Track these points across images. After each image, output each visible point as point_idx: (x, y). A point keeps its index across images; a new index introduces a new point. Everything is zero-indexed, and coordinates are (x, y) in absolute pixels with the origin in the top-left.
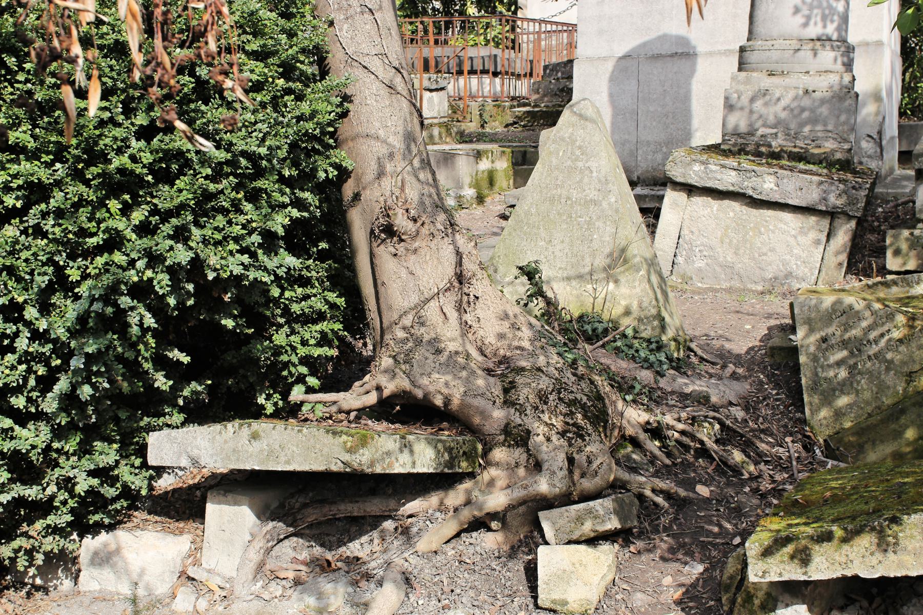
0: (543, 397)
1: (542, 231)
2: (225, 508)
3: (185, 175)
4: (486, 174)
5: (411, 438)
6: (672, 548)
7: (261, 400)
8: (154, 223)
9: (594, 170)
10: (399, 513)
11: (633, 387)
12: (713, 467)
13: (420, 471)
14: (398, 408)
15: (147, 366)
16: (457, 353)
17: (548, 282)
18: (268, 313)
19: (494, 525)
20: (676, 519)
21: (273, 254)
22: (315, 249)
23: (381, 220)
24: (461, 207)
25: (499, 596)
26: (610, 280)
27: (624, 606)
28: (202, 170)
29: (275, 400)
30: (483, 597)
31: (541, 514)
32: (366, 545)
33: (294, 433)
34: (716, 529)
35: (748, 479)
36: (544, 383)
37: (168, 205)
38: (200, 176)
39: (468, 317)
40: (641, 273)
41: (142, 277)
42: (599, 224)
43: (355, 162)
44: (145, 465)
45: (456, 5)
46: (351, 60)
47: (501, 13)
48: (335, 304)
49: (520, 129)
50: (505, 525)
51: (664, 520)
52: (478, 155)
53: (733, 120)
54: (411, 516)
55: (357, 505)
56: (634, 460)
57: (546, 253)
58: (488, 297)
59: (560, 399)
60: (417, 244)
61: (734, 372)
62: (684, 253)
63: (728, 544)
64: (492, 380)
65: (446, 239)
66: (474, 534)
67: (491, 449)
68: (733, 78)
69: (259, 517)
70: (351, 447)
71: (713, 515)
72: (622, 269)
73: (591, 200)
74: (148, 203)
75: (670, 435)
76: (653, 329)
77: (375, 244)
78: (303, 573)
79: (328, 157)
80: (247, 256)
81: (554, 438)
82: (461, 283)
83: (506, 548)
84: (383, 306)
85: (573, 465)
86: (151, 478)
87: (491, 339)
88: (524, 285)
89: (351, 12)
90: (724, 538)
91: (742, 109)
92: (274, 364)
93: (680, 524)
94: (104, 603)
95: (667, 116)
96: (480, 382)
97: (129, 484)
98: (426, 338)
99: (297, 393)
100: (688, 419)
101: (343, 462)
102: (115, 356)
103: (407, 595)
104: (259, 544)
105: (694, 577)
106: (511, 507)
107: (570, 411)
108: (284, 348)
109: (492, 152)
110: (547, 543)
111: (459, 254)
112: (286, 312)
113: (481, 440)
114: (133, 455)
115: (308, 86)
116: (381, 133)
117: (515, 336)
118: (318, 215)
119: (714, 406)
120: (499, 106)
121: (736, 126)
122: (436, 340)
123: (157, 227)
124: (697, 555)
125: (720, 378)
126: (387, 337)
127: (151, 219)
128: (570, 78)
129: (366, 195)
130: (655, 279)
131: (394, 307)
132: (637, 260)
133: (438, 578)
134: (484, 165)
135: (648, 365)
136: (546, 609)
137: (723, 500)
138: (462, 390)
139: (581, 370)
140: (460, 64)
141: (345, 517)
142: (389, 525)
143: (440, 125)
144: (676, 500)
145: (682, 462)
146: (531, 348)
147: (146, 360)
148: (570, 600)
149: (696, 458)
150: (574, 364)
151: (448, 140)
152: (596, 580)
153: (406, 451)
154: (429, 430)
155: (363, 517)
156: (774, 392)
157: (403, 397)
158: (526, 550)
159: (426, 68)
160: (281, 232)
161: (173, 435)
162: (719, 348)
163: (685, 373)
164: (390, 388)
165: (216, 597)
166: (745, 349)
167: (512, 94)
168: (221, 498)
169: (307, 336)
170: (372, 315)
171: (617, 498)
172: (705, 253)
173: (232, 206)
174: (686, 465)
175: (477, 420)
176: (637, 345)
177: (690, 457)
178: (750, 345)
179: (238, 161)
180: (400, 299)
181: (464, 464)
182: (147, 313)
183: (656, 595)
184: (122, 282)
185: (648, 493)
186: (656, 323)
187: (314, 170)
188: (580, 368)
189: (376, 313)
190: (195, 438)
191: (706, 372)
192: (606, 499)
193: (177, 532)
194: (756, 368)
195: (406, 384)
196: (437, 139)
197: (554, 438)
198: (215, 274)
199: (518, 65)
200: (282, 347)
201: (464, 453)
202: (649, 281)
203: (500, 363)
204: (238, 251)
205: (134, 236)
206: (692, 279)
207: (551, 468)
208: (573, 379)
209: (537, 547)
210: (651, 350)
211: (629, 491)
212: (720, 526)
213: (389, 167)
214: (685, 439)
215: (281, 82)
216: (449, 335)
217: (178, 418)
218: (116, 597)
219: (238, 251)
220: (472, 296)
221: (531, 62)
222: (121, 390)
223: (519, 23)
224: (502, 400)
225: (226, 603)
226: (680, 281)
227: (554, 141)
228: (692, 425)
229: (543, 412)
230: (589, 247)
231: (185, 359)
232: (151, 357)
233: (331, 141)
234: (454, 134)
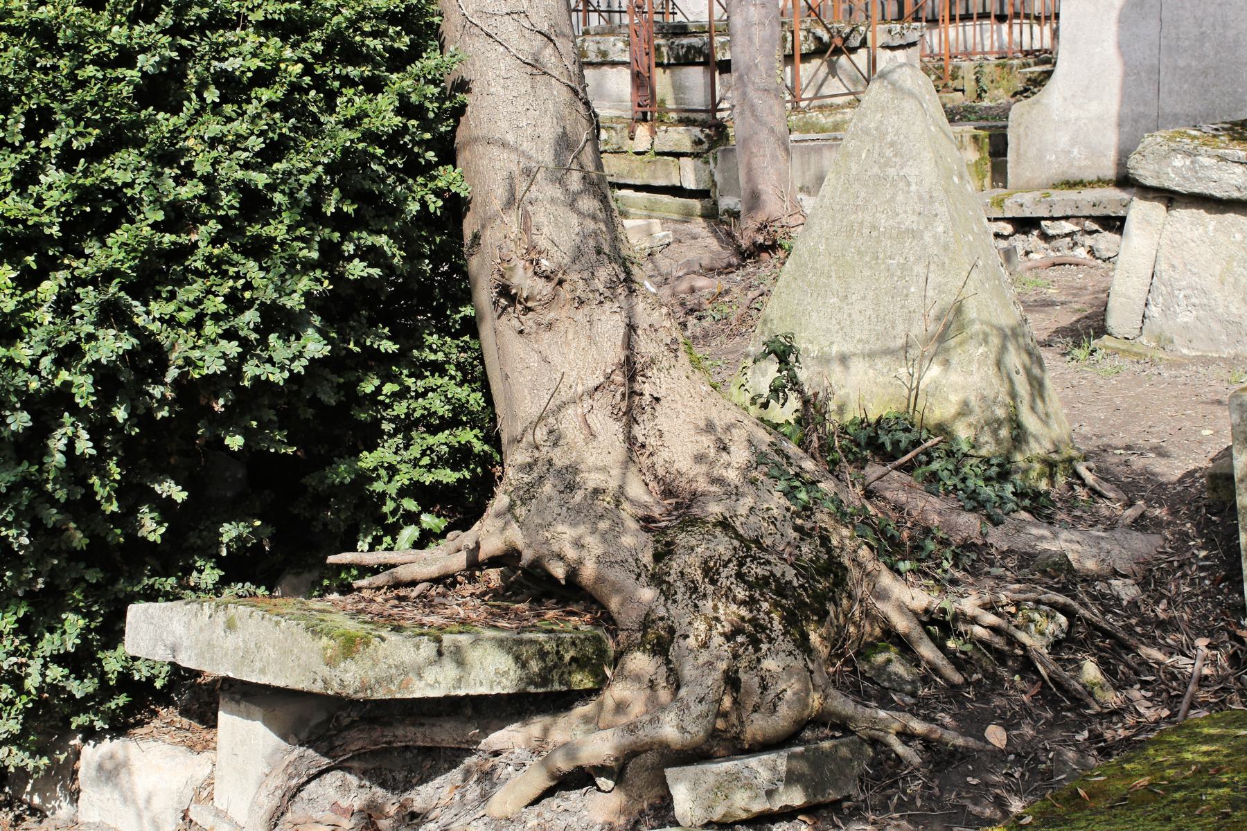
0: (710, 573)
9: (912, 180)
10: (480, 747)
13: (472, 692)
19: (602, 782)
21: (293, 338)
31: (670, 773)
35: (1097, 715)
54: (496, 754)
55: (421, 729)
57: (839, 316)
60: (552, 315)
62: (1161, 300)
73: (907, 230)
80: (235, 343)
87: (684, 464)
95: (1205, 73)
98: (559, 463)
107: (751, 597)
111: (631, 328)
116: (510, 138)
120: (1003, 66)
122: (573, 469)
132: (977, 327)
135: (976, 503)
137: (1028, 753)
156: (1203, 554)
166: (1178, 474)
167: (1026, 47)
172: (1194, 300)
175: (614, 604)
178: (1191, 467)
186: (1004, 433)
194: (1184, 510)
206: (1172, 342)
214: (999, 642)
219: (222, 336)
226: (1153, 344)
231: (180, 496)
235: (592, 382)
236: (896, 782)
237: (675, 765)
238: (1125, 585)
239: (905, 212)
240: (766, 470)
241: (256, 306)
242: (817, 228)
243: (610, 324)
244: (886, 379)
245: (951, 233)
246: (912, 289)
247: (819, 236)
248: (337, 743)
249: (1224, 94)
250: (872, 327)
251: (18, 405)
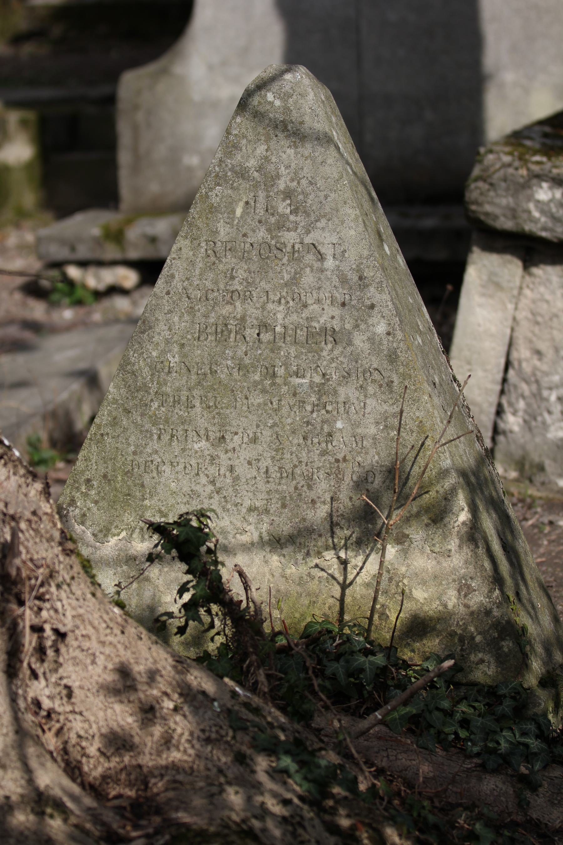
57: (212, 470)
58: (90, 631)
62: (521, 404)
73: (324, 330)
220: (48, 632)
226: (513, 474)
230: (324, 453)
239: (318, 301)
242: (162, 327)
245: (399, 335)
246: (339, 425)
247: (167, 342)
250: (272, 486)
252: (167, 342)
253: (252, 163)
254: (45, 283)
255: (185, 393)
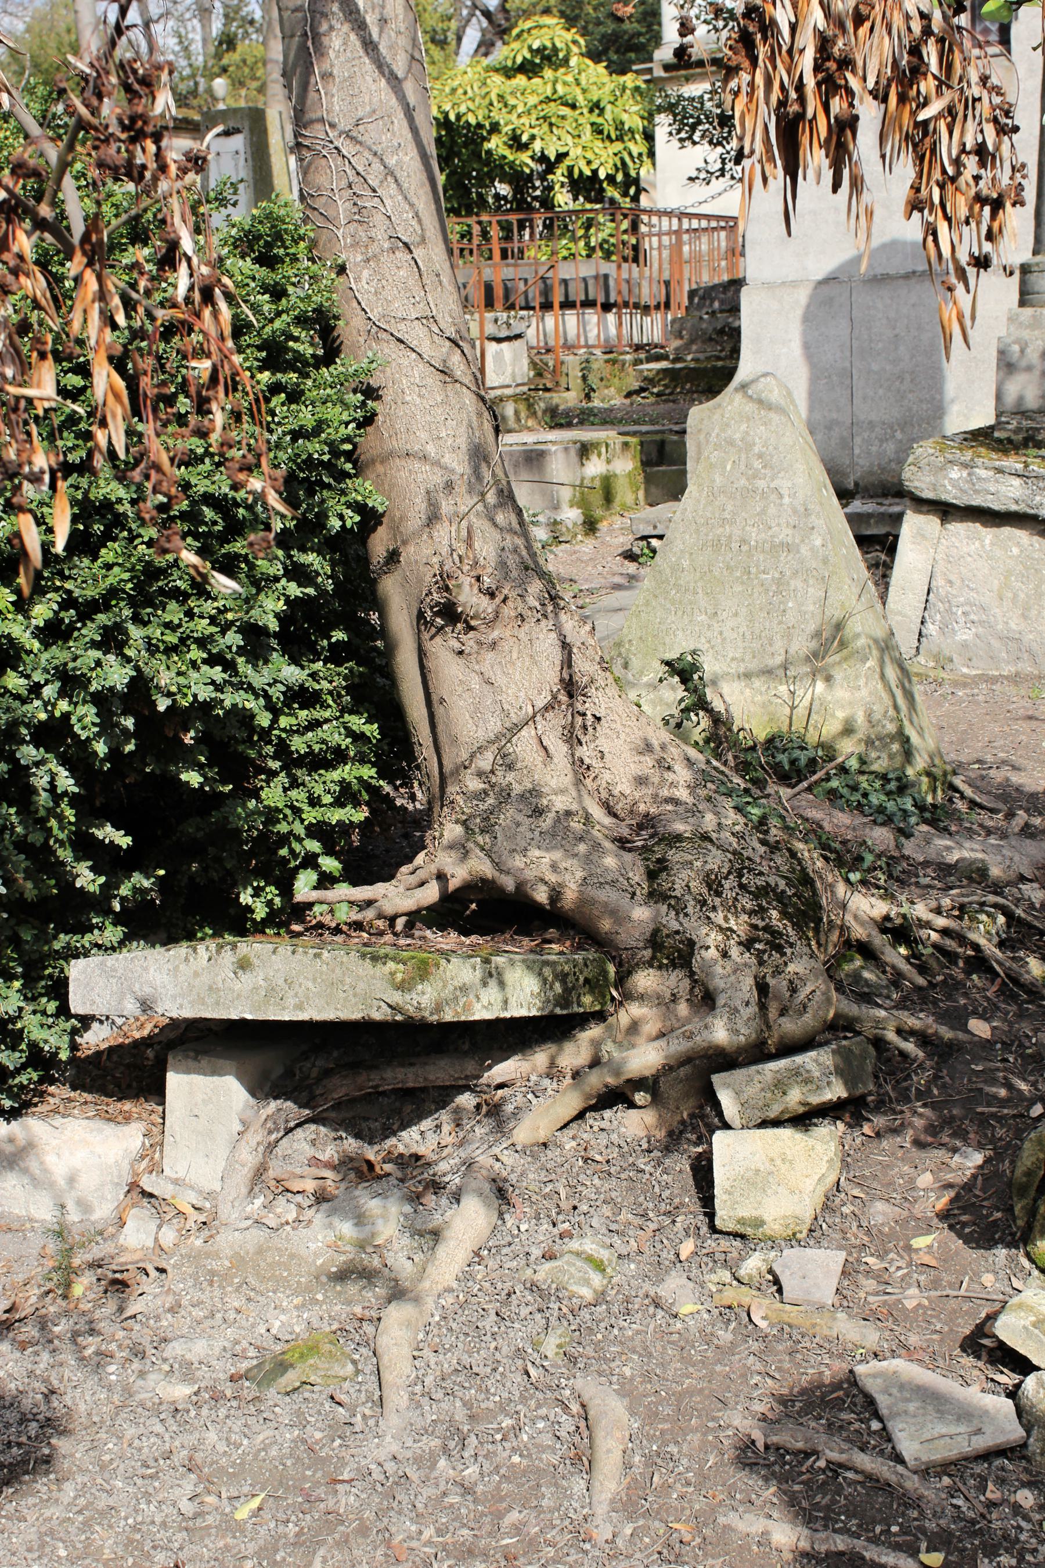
0: (713, 884)
1: (702, 601)
2: (198, 1081)
3: (115, 539)
4: (597, 484)
5: (499, 960)
6: (932, 1125)
7: (246, 898)
8: (67, 621)
9: (785, 492)
10: (482, 1081)
11: (860, 859)
12: (995, 988)
14: (474, 906)
15: (65, 854)
16: (568, 813)
17: (714, 683)
18: (252, 754)
19: (640, 1097)
20: (936, 1077)
21: (261, 663)
22: (325, 643)
23: (436, 596)
24: (557, 540)
25: (651, 1214)
26: (818, 676)
27: (855, 1224)
28: (141, 531)
29: (269, 897)
30: (625, 1216)
31: (716, 1079)
32: (429, 1135)
33: (307, 960)
34: (1003, 1092)
36: (716, 861)
37: (91, 593)
38: (140, 540)
39: (583, 752)
40: (868, 664)
41: (52, 712)
42: (797, 583)
43: (389, 498)
44: (64, 1011)
45: (535, 188)
46: (376, 330)
47: (612, 201)
48: (363, 734)
49: (652, 399)
50: (657, 1098)
51: (920, 1080)
52: (585, 450)
53: (1013, 389)
54: (501, 1086)
55: (412, 1070)
56: (866, 980)
57: (709, 634)
58: (616, 718)
59: (742, 886)
60: (495, 634)
61: (1027, 825)
63: (1022, 1116)
64: (628, 857)
65: (544, 622)
66: (607, 1114)
67: (629, 973)
68: (1011, 319)
69: (253, 1094)
70: (403, 980)
71: (998, 1069)
72: (837, 658)
73: (782, 544)
74: (57, 589)
75: (924, 937)
76: (891, 757)
77: (426, 636)
78: (329, 1182)
79: (343, 492)
80: (219, 668)
81: (735, 952)
82: (571, 696)
83: (660, 1134)
84: (443, 738)
85: (766, 996)
86: (74, 1032)
87: (624, 787)
88: (673, 688)
89: (374, 248)
90: (1016, 1106)
91: (1029, 368)
92: (264, 836)
93: (944, 1086)
94: (10, 1235)
96: (610, 861)
97: (42, 1045)
98: (517, 789)
99: (304, 886)
100: (953, 908)
101: (390, 1006)
102: (14, 843)
103: (501, 1215)
104: (256, 1137)
105: (968, 1173)
106: (668, 1069)
107: (759, 906)
108: (280, 811)
109: (607, 446)
110: (727, 1126)
112: (282, 750)
113: (614, 958)
114: (42, 995)
115: (307, 376)
116: (431, 449)
117: (663, 780)
118: (330, 588)
119: (995, 884)
120: (614, 362)
121: (1021, 399)
123: (71, 628)
124: (972, 1136)
125: (1004, 836)
126: (452, 789)
127: (62, 614)
128: (735, 309)
129: (408, 554)
130: (892, 673)
131: (462, 739)
132: (862, 642)
133: (550, 1186)
134: (595, 467)
135: (883, 817)
136: (728, 1234)
137: (1013, 1042)
138: (580, 874)
139: (775, 833)
140: (547, 291)
141: (395, 1091)
142: (466, 1100)
143: (516, 398)
144: (937, 1046)
145: (944, 981)
146: (690, 800)
147: (62, 844)
148: (766, 1218)
149: (968, 973)
150: (762, 822)
151: (530, 423)
152: (809, 1184)
153: (493, 983)
154: (527, 942)
155: (423, 1090)
157: (481, 889)
158: (694, 1137)
159: (489, 304)
160: (274, 625)
161: (109, 964)
162: (1000, 784)
163: (946, 829)
164: (459, 875)
165: (190, 1224)
167: (636, 340)
168: (191, 1063)
169: (318, 790)
170: (425, 752)
171: (840, 1047)
172: (973, 617)
173: (192, 587)
174: (952, 987)
175: (606, 925)
176: (865, 785)
177: (957, 972)
179: (201, 513)
180: (470, 725)
181: (587, 999)
182: (60, 768)
183: (906, 1205)
184: (23, 722)
185: (891, 1036)
186: (895, 747)
187: (322, 516)
188: (774, 831)
189: (432, 749)
190: (146, 969)
191: (981, 825)
192: (822, 1051)
193: (120, 1118)
195: (484, 868)
196: (512, 423)
197: (735, 952)
198: (168, 702)
199: (645, 291)
200: (278, 810)
201: (587, 981)
202: (883, 676)
203: (641, 827)
204: (205, 661)
205: (36, 645)
207: (732, 1003)
208: (762, 849)
209: (712, 1132)
210: (888, 794)
211: (858, 1033)
212: (1009, 1086)
213: (446, 507)
214: (950, 944)
215: (265, 377)
216: (553, 783)
217: (112, 934)
218: (28, 1226)
219: (205, 661)
220: (589, 717)
221: (667, 284)
222: (22, 894)
223: (645, 218)
224: (645, 891)
225: (206, 1233)
226: (932, 664)
227: (717, 447)
228: (960, 918)
229: (714, 909)
230: (780, 623)
231: (124, 841)
232: (69, 838)
233: (348, 466)
234: (540, 414)
235: (540, 703)
236: (909, 1075)
237: (718, 1072)
238: (1033, 889)
239: (778, 525)
240: (713, 787)
241: (235, 629)
242: (678, 542)
243: (547, 644)
244: (765, 698)
245: (830, 546)
246: (790, 605)
248: (318, 1092)
249: (921, 401)
250: (746, 644)
251: (28, 738)
252: (682, 551)
253: (738, 436)
254: (636, 550)
255: (692, 584)
